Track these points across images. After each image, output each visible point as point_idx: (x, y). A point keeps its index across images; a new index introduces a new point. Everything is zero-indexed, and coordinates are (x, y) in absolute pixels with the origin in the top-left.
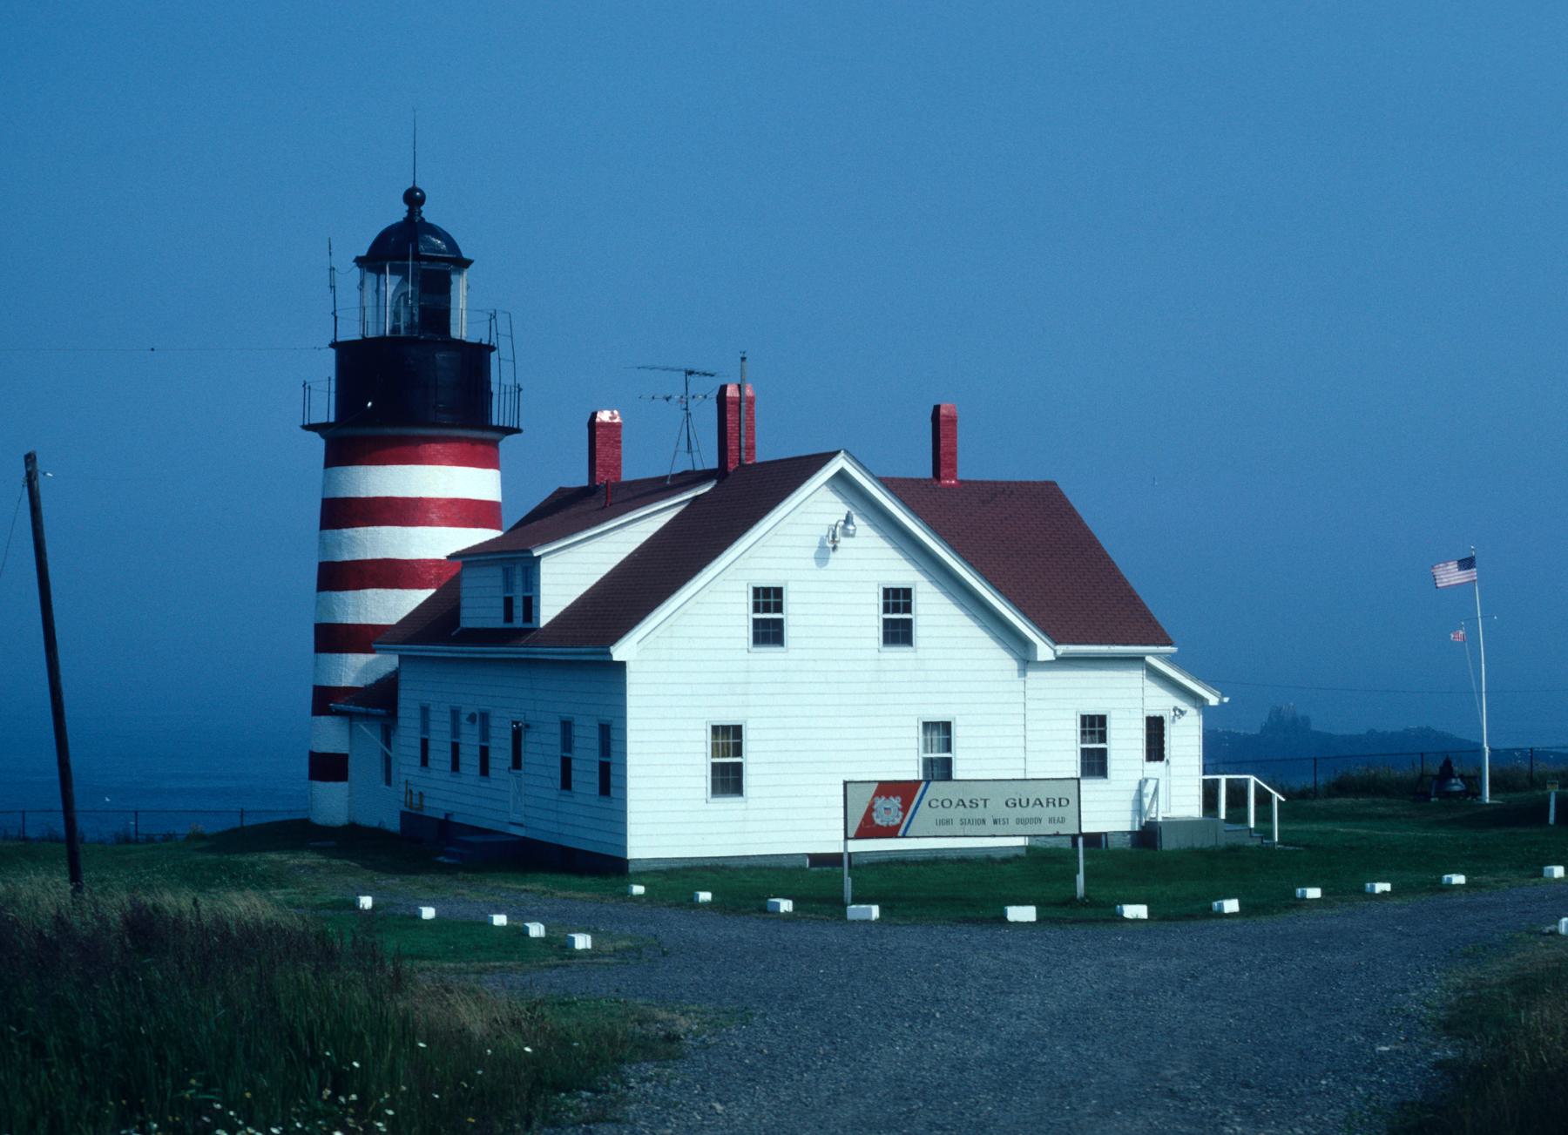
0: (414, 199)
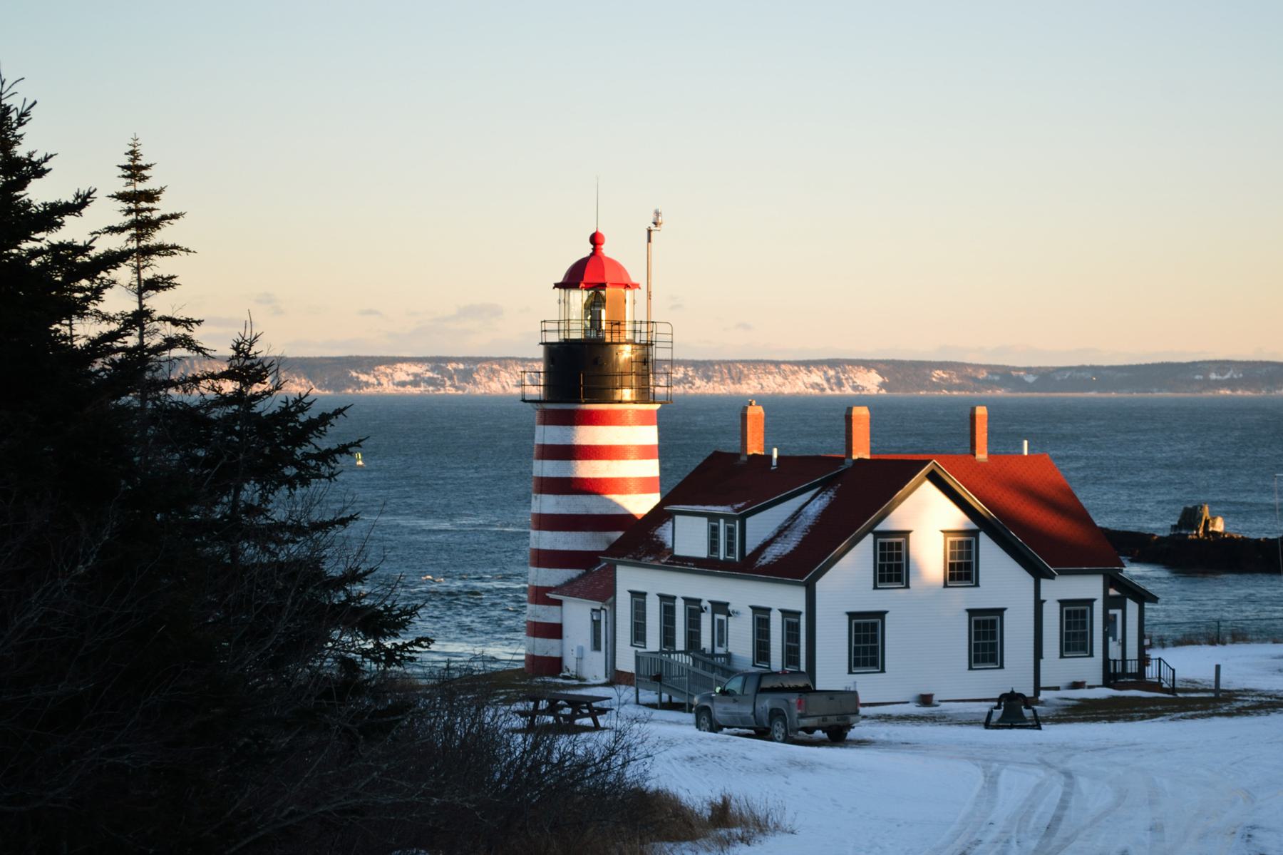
0: (595, 240)
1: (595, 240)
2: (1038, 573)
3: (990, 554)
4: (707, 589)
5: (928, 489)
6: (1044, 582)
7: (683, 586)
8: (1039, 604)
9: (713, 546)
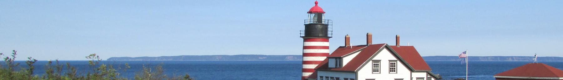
0: (316, 3)
1: (316, 3)
2: (412, 71)
3: (400, 65)
4: (335, 75)
5: (385, 50)
6: (413, 73)
7: (330, 74)
8: (411, 78)
9: (336, 65)
